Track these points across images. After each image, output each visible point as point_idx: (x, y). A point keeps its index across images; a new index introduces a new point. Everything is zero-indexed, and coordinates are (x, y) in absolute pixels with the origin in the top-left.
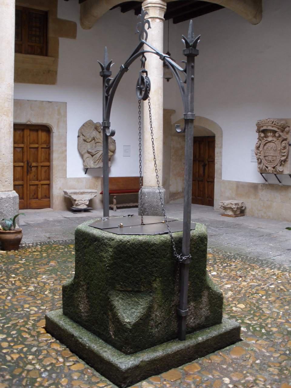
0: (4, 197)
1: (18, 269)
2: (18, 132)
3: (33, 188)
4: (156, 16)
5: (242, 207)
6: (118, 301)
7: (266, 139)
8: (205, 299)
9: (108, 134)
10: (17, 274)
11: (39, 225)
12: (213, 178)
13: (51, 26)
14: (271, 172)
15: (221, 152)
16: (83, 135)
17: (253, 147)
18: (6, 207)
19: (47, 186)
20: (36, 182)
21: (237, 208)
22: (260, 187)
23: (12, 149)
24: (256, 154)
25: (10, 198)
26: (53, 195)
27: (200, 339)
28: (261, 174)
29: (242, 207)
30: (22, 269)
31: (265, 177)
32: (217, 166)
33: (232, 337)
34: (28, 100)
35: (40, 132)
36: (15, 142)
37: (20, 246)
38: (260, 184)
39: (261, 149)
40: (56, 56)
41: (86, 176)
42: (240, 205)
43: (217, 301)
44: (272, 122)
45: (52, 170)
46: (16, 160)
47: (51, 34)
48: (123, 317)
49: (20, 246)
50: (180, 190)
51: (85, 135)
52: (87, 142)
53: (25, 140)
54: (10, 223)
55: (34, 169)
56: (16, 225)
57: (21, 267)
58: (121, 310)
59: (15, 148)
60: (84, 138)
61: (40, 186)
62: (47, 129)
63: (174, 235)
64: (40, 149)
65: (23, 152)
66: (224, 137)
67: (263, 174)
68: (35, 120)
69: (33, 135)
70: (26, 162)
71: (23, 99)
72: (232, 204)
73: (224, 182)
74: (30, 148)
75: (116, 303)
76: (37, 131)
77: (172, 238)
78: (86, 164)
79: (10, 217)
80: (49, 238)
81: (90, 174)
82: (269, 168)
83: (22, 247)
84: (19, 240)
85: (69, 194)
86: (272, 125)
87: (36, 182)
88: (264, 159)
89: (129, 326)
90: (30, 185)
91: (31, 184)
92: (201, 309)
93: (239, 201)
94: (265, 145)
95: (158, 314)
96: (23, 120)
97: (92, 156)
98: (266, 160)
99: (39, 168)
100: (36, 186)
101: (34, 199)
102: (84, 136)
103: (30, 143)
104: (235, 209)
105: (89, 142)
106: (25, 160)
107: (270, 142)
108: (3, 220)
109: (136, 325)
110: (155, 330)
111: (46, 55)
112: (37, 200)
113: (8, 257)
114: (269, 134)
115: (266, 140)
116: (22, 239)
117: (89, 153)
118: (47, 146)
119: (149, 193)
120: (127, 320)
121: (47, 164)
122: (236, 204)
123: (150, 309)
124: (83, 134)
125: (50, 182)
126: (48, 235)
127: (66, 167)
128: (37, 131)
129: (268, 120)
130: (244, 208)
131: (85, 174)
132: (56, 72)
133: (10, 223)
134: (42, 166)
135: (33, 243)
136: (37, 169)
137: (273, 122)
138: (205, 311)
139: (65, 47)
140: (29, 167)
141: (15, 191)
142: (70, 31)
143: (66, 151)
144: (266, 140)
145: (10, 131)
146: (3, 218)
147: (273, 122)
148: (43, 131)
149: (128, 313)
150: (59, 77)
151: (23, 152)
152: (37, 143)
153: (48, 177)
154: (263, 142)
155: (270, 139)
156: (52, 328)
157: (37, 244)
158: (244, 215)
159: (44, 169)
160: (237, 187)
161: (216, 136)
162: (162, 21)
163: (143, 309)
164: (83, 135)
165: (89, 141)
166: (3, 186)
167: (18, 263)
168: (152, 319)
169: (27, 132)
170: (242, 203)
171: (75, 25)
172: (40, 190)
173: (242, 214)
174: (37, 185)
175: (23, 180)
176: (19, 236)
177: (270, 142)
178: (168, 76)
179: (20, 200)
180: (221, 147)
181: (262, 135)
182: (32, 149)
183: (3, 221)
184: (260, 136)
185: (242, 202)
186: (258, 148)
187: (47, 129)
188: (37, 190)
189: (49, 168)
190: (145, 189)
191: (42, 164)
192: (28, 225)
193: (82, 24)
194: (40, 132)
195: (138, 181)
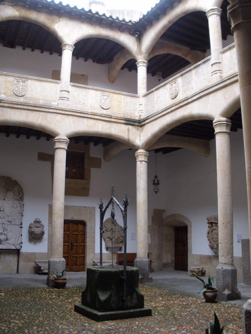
0: (58, 260)
1: (64, 295)
2: (66, 225)
3: (74, 259)
4: (143, 160)
5: (203, 271)
6: (100, 293)
7: (212, 228)
8: (135, 296)
9: (102, 232)
10: (63, 296)
11: (77, 279)
12: (187, 252)
13: (86, 161)
14: (216, 248)
15: (191, 237)
16: (105, 227)
17: (206, 232)
18: (59, 266)
19: (83, 258)
20: (76, 255)
21: (199, 271)
22: (213, 258)
23: (63, 236)
24: (208, 237)
25: (61, 261)
26: (86, 263)
27: (132, 311)
28: (212, 249)
29: (203, 271)
30: (66, 295)
31: (214, 251)
32: (189, 245)
33: (148, 313)
34: (72, 206)
35: (79, 225)
36: (64, 231)
37: (65, 287)
38: (212, 256)
39: (210, 234)
40: (89, 179)
41: (107, 252)
42: (201, 270)
43: (141, 299)
44: (214, 218)
45: (86, 248)
46: (64, 242)
47: (86, 167)
48: (101, 298)
49: (65, 287)
50: (170, 261)
51: (106, 227)
52: (108, 231)
53: (70, 230)
54: (61, 274)
55: (75, 247)
56: (64, 276)
57: (65, 294)
58: (100, 296)
59: (64, 234)
60: (106, 229)
61: (79, 258)
62: (83, 223)
63: (120, 269)
64: (79, 235)
65: (69, 237)
66: (192, 227)
67: (213, 249)
68: (77, 218)
69: (75, 226)
70: (70, 243)
71: (69, 205)
72: (195, 269)
73: (193, 255)
74: (73, 234)
75: (99, 293)
76: (77, 224)
77: (119, 270)
78: (107, 245)
79: (61, 271)
80: (81, 285)
81: (109, 251)
82: (215, 246)
83: (67, 288)
84: (65, 283)
85: (96, 263)
86: (215, 219)
87: (76, 255)
88: (212, 241)
89: (102, 301)
90: (73, 257)
91: (73, 256)
92: (133, 300)
93: (200, 267)
94: (212, 231)
95: (114, 298)
96: (69, 218)
97: (111, 240)
98: (213, 240)
99: (78, 247)
100: (76, 258)
101: (75, 265)
102: (106, 228)
103: (73, 232)
104: (197, 272)
105: (109, 231)
106: (70, 241)
107: (214, 229)
108: (57, 273)
109: (105, 301)
110: (113, 305)
111: (83, 179)
112: (77, 266)
113: (59, 291)
114: (214, 225)
115: (213, 229)
116: (67, 284)
117: (109, 238)
118: (83, 233)
119: (139, 261)
120: (102, 299)
121: (83, 244)
122: (198, 269)
123: (111, 295)
124: (105, 226)
125: (85, 255)
126: (81, 284)
127: (95, 247)
128: (77, 224)
129: (212, 216)
130: (204, 271)
131: (107, 250)
132: (89, 189)
133: (61, 274)
134: (80, 246)
135: (72, 287)
136: (77, 247)
137: (215, 218)
138: (135, 301)
139: (94, 173)
140: (72, 246)
141: (63, 258)
142: (97, 163)
143: (95, 236)
144: (213, 229)
145: (62, 226)
146: (57, 272)
147: (215, 218)
148: (80, 224)
149: (103, 297)
150: (91, 192)
151: (69, 237)
152: (77, 232)
153: (84, 253)
154: (211, 230)
155: (214, 228)
156: (77, 309)
157: (74, 287)
158: (204, 276)
159: (81, 247)
160: (201, 258)
161: (188, 226)
162: (146, 162)
163: (108, 295)
164: (105, 227)
165: (109, 231)
166: (58, 255)
167: (64, 293)
168: (112, 300)
169: (71, 225)
170: (203, 268)
171: (100, 160)
172: (78, 260)
173: (203, 275)
174: (77, 257)
175: (68, 254)
176: (65, 281)
177: (214, 229)
178: (157, 191)
179: (67, 266)
180: (191, 233)
181: (210, 225)
182: (74, 235)
183: (57, 273)
184: (209, 226)
185: (202, 267)
186: (208, 233)
187: (83, 223)
188: (77, 260)
189: (84, 247)
190: (137, 259)
191: (80, 244)
192: (70, 279)
193: (104, 159)
194: (79, 225)
195: (134, 255)
